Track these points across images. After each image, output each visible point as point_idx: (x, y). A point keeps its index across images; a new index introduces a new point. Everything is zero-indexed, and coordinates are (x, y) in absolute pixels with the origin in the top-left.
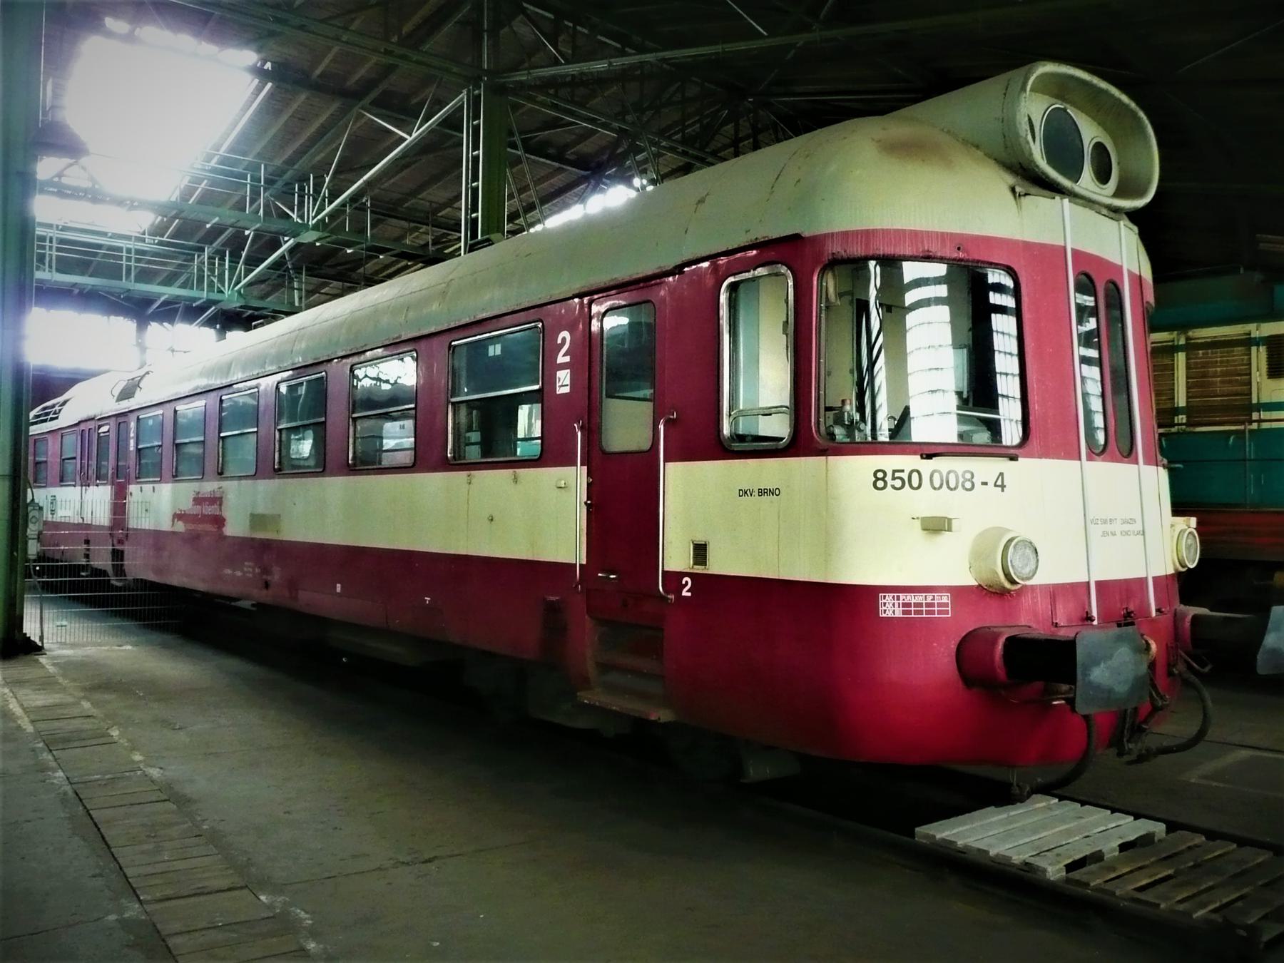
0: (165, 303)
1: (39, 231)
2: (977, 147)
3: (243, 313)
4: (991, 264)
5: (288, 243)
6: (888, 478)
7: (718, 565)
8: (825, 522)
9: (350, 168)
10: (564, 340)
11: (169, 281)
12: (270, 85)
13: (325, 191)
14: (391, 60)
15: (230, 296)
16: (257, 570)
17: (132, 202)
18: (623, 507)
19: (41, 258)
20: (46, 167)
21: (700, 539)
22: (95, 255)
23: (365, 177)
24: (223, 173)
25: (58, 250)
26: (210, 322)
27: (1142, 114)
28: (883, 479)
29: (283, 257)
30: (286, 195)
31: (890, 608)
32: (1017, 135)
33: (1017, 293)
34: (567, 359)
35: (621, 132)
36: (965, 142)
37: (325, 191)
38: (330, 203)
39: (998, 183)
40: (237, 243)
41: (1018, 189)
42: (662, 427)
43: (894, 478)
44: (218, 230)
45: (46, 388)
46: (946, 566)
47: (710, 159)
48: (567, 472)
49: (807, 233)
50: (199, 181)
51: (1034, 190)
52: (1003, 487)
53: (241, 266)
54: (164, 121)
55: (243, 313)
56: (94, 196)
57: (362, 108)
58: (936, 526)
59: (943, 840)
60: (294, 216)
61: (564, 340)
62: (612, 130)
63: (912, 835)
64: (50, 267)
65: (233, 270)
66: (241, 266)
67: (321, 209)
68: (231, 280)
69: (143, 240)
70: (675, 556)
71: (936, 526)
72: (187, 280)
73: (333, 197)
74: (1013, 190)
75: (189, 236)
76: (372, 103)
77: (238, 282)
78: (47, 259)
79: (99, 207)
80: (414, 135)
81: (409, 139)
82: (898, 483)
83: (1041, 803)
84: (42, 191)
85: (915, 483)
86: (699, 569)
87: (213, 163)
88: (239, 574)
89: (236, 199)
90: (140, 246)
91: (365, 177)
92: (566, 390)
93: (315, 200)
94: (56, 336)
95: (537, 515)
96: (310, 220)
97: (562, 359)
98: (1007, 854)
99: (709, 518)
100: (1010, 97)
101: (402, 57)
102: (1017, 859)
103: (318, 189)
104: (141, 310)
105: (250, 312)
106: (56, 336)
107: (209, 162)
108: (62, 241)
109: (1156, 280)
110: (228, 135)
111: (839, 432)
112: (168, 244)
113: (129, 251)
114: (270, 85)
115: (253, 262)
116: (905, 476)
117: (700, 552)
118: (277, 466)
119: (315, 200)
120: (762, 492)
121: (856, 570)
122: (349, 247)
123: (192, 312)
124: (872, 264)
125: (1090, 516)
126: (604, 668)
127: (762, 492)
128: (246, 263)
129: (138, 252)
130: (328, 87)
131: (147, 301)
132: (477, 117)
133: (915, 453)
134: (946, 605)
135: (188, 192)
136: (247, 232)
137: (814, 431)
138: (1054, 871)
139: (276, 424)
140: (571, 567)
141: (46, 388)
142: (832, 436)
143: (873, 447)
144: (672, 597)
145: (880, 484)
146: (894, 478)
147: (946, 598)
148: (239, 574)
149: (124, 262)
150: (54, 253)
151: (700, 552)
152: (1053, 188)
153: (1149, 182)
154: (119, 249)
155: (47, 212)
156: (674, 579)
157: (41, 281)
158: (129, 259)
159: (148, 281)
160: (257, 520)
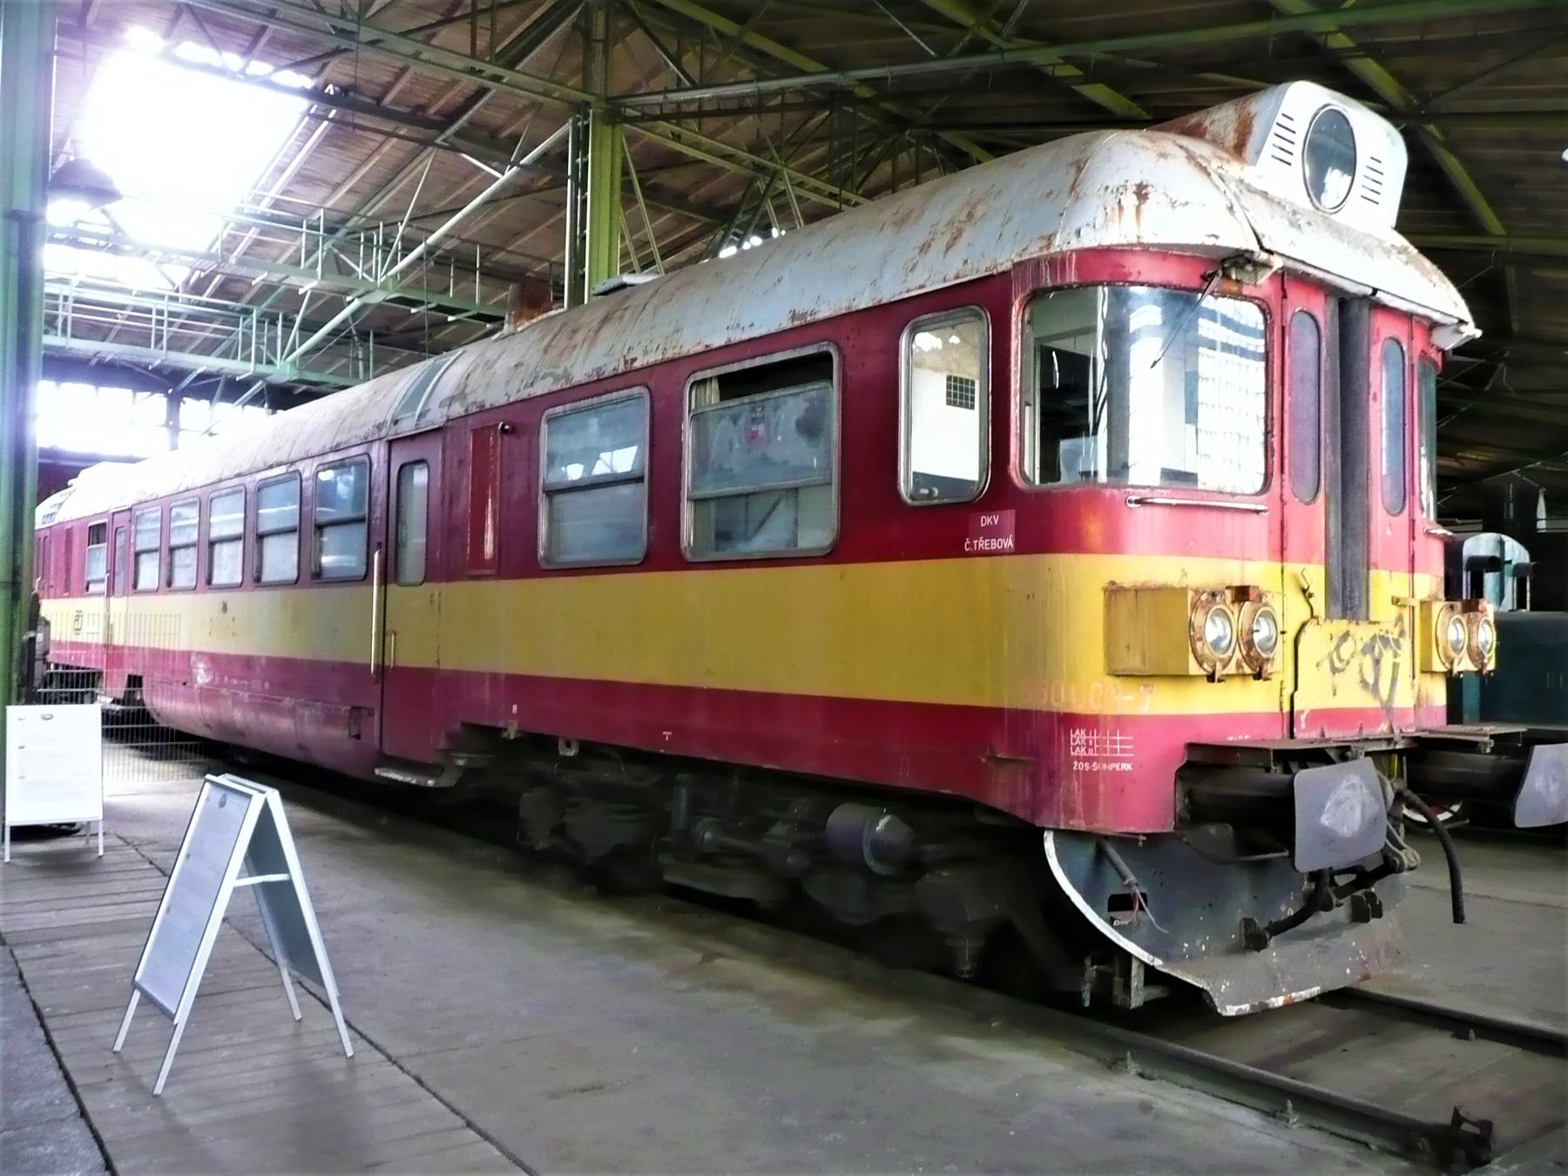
0: (202, 376)
1: (50, 288)
3: (293, 388)
9: (428, 216)
11: (207, 348)
13: (397, 243)
15: (283, 370)
17: (165, 252)
19: (51, 322)
20: (60, 211)
22: (114, 316)
24: (273, 218)
25: (75, 310)
26: (256, 400)
29: (345, 321)
37: (397, 243)
38: (404, 256)
44: (268, 289)
45: (56, 475)
47: (854, 198)
50: (246, 228)
51: (353, 771)
54: (190, 152)
55: (293, 388)
56: (113, 244)
60: (359, 270)
62: (739, 162)
64: (64, 332)
68: (283, 348)
69: (175, 299)
72: (230, 347)
73: (407, 250)
75: (228, 298)
77: (293, 350)
78: (60, 322)
79: (122, 259)
81: (502, 179)
83: (1126, 585)
84: (52, 240)
89: (290, 251)
90: (175, 307)
93: (386, 253)
94: (62, 415)
96: (378, 281)
101: (497, 79)
104: (172, 384)
105: (304, 387)
106: (62, 415)
107: (259, 203)
108: (77, 301)
112: (207, 305)
113: (160, 313)
115: (309, 327)
119: (386, 253)
122: (452, 314)
123: (234, 389)
124: (966, 967)
128: (301, 329)
129: (171, 314)
130: (426, 122)
131: (176, 375)
135: (230, 244)
136: (301, 291)
141: (56, 475)
149: (153, 325)
150: (71, 315)
154: (149, 311)
155: (59, 266)
157: (48, 348)
158: (160, 322)
159: (181, 349)
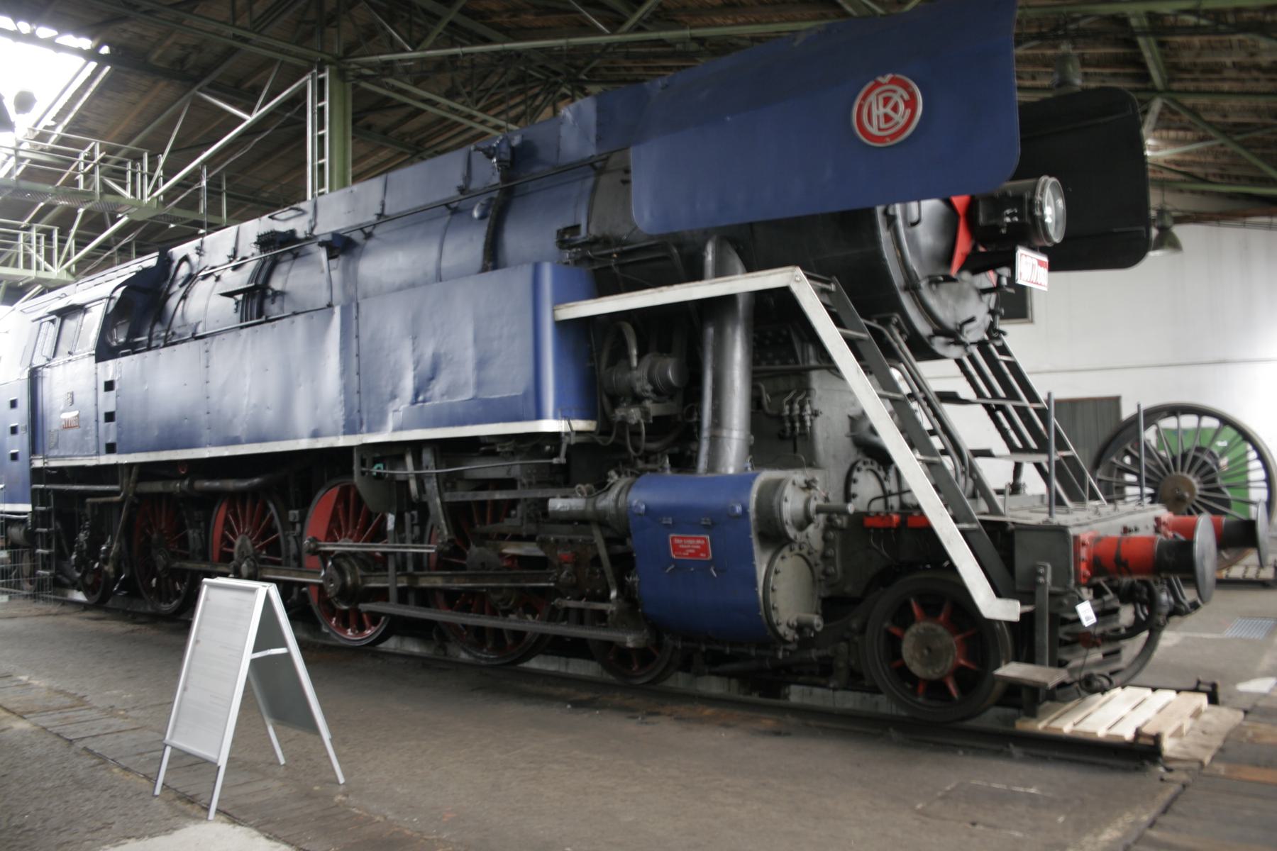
4: (168, 241)
12: (108, 68)
13: (159, 172)
14: (236, 44)
23: (507, 46)
30: (119, 175)
38: (165, 182)
53: (71, 242)
57: (200, 90)
65: (62, 242)
66: (71, 242)
67: (156, 187)
76: (210, 86)
80: (255, 115)
81: (249, 119)
87: (50, 144)
91: (507, 46)
92: (731, 471)
93: (150, 178)
103: (152, 169)
110: (81, 96)
114: (108, 68)
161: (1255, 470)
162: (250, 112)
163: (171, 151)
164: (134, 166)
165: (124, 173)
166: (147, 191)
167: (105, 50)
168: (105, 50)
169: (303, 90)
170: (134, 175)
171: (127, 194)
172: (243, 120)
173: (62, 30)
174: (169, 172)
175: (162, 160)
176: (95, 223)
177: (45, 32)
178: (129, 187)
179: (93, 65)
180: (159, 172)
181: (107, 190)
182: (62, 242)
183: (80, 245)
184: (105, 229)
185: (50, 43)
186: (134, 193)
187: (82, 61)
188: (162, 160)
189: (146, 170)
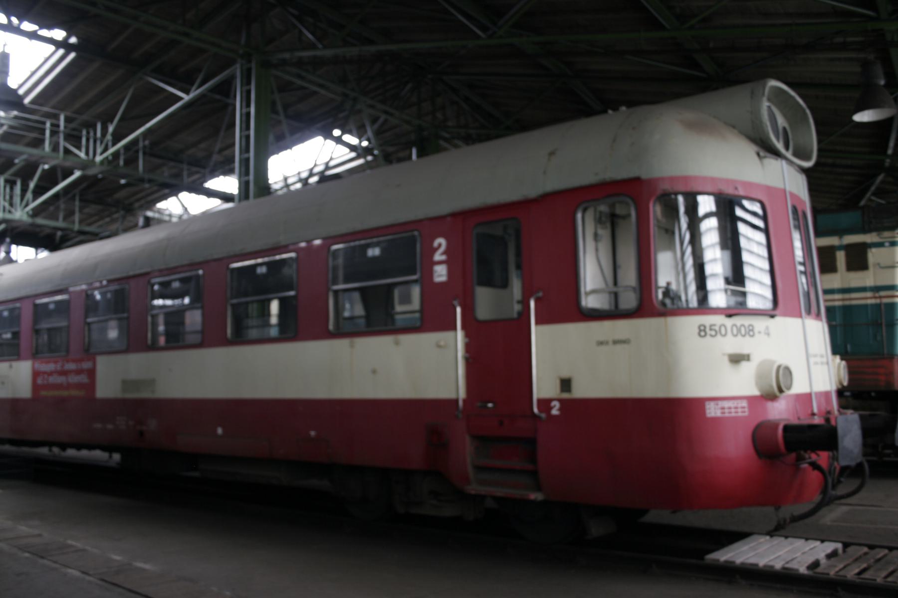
2: (734, 127)
5: (77, 174)
6: (708, 330)
7: (580, 391)
8: (667, 359)
10: (440, 245)
12: (72, 55)
16: (131, 423)
18: (499, 357)
21: (565, 374)
27: (808, 112)
28: (704, 330)
31: (712, 411)
32: (761, 122)
33: (765, 218)
34: (444, 258)
35: (345, 95)
36: (726, 123)
39: (749, 150)
40: (26, 172)
41: (762, 154)
42: (532, 304)
43: (711, 329)
46: (741, 384)
48: (449, 335)
49: (644, 176)
51: (768, 155)
52: (768, 334)
53: (29, 195)
58: (737, 359)
59: (726, 562)
61: (440, 245)
63: (703, 559)
67: (106, 149)
70: (543, 385)
71: (737, 359)
74: (758, 154)
77: (27, 205)
80: (192, 95)
81: (186, 98)
82: (713, 333)
85: (723, 332)
86: (565, 396)
88: (110, 426)
91: (148, 125)
93: (101, 143)
95: (427, 366)
97: (438, 257)
98: (771, 564)
99: (562, 360)
100: (755, 97)
102: (778, 566)
109: (815, 211)
111: (668, 301)
114: (72, 55)
116: (717, 328)
117: (566, 384)
118: (137, 341)
120: (615, 342)
121: (692, 386)
122: (123, 178)
125: (811, 351)
126: (479, 469)
127: (615, 342)
132: (249, 83)
133: (721, 314)
134: (744, 408)
137: (648, 303)
138: (803, 570)
139: (86, 317)
140: (456, 401)
142: (664, 304)
143: (688, 311)
144: (543, 415)
145: (703, 333)
146: (711, 329)
147: (744, 404)
148: (110, 426)
151: (566, 384)
152: (776, 154)
153: (811, 151)
156: (545, 404)
160: (127, 384)
161: (714, 260)
162: (187, 92)
163: (121, 120)
164: (88, 133)
165: (80, 138)
166: (99, 150)
167: (73, 40)
168: (73, 40)
169: (232, 78)
170: (88, 140)
171: (82, 155)
172: (181, 99)
173: (21, 19)
174: (117, 138)
175: (111, 129)
176: (50, 178)
177: (27, 26)
178: (84, 149)
179: (61, 52)
180: (109, 137)
181: (67, 151)
182: (24, 191)
183: (35, 197)
184: (56, 184)
185: (33, 36)
186: (87, 153)
187: (52, 48)
188: (111, 129)
189: (99, 134)
